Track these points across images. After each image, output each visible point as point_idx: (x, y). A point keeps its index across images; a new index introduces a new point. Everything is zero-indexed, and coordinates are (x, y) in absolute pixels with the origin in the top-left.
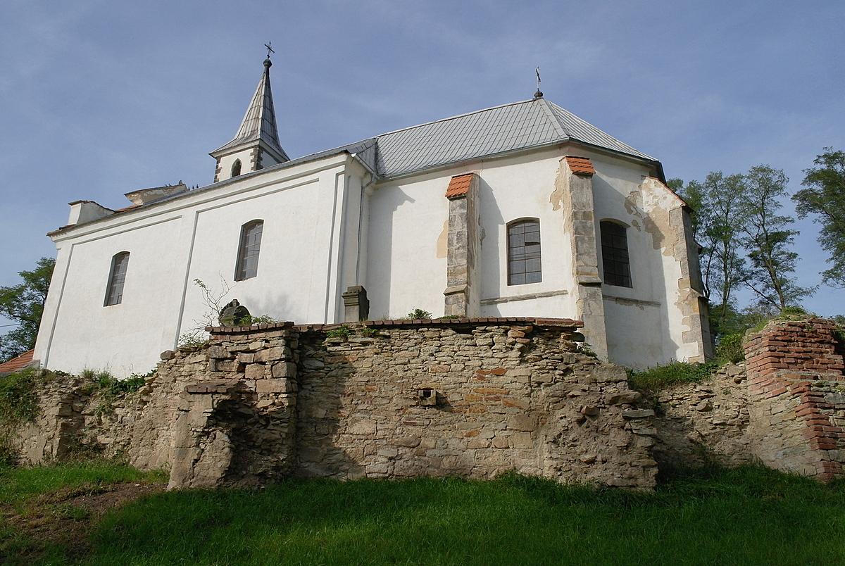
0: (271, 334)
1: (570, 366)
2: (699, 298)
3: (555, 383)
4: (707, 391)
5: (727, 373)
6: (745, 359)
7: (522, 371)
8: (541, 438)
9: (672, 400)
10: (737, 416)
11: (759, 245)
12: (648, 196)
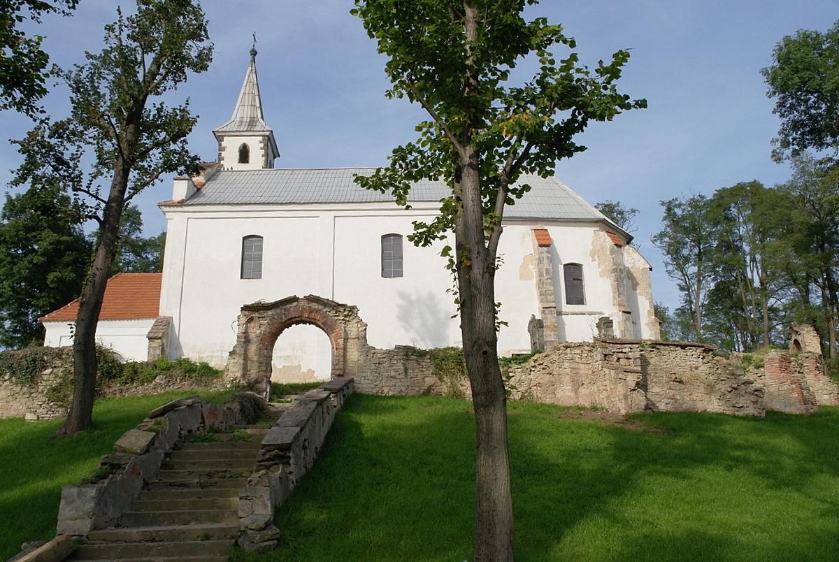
0: (634, 345)
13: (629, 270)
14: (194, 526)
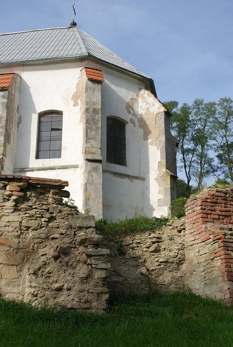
1: (54, 215)
2: (171, 176)
3: (41, 228)
4: (158, 238)
5: (173, 225)
6: (186, 215)
7: (15, 217)
8: (25, 272)
9: (132, 243)
10: (177, 256)
11: (223, 150)
12: (142, 103)
13: (142, 118)
14: (202, 238)
